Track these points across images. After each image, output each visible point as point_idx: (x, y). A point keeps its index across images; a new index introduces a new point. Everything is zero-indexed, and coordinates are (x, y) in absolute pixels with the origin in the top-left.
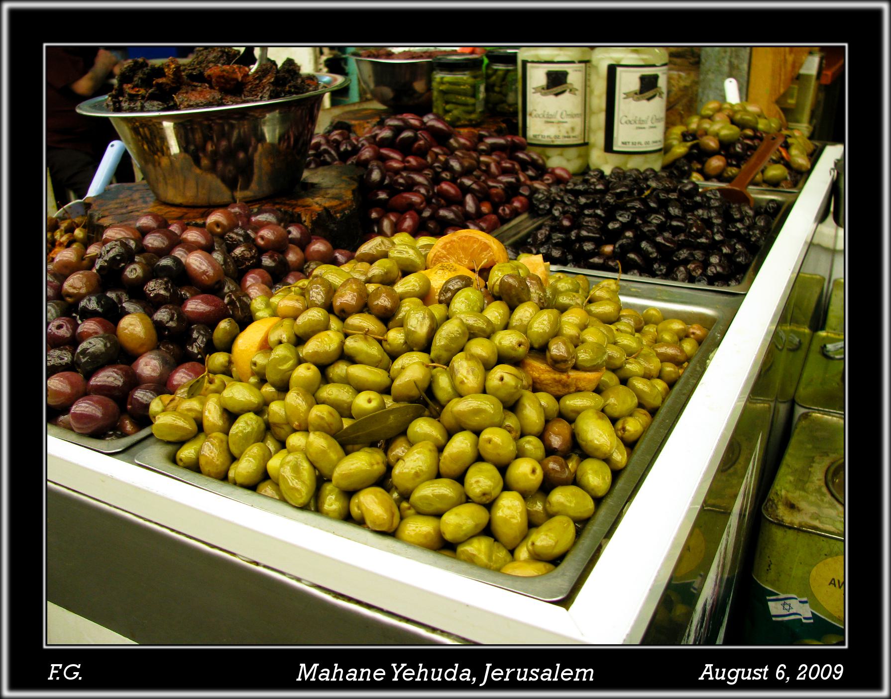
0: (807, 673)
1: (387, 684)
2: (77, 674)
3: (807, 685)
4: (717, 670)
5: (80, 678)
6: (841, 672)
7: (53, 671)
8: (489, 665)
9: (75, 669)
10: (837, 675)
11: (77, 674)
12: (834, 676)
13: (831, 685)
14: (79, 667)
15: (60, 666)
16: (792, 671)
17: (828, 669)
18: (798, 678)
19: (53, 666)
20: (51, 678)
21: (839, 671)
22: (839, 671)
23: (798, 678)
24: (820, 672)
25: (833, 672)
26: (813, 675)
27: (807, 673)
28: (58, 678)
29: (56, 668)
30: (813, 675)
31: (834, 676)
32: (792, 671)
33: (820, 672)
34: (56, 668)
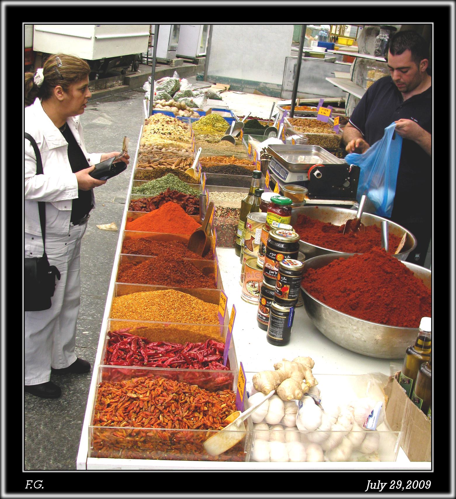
0: (411, 485)
1: (386, 490)
2: (41, 485)
3: (412, 491)
4: (372, 484)
5: (43, 488)
6: (430, 485)
7: (28, 484)
8: (369, 481)
9: (40, 483)
10: (427, 487)
11: (41, 485)
12: (426, 487)
13: (424, 491)
14: (42, 482)
15: (32, 481)
16: (404, 485)
17: (422, 483)
18: (390, 488)
19: (28, 481)
20: (27, 488)
21: (429, 484)
22: (429, 484)
23: (390, 488)
24: (419, 485)
25: (426, 485)
26: (415, 487)
27: (411, 485)
28: (31, 488)
29: (29, 482)
30: (415, 486)
31: (426, 487)
32: (404, 485)
33: (419, 485)
34: (29, 482)
